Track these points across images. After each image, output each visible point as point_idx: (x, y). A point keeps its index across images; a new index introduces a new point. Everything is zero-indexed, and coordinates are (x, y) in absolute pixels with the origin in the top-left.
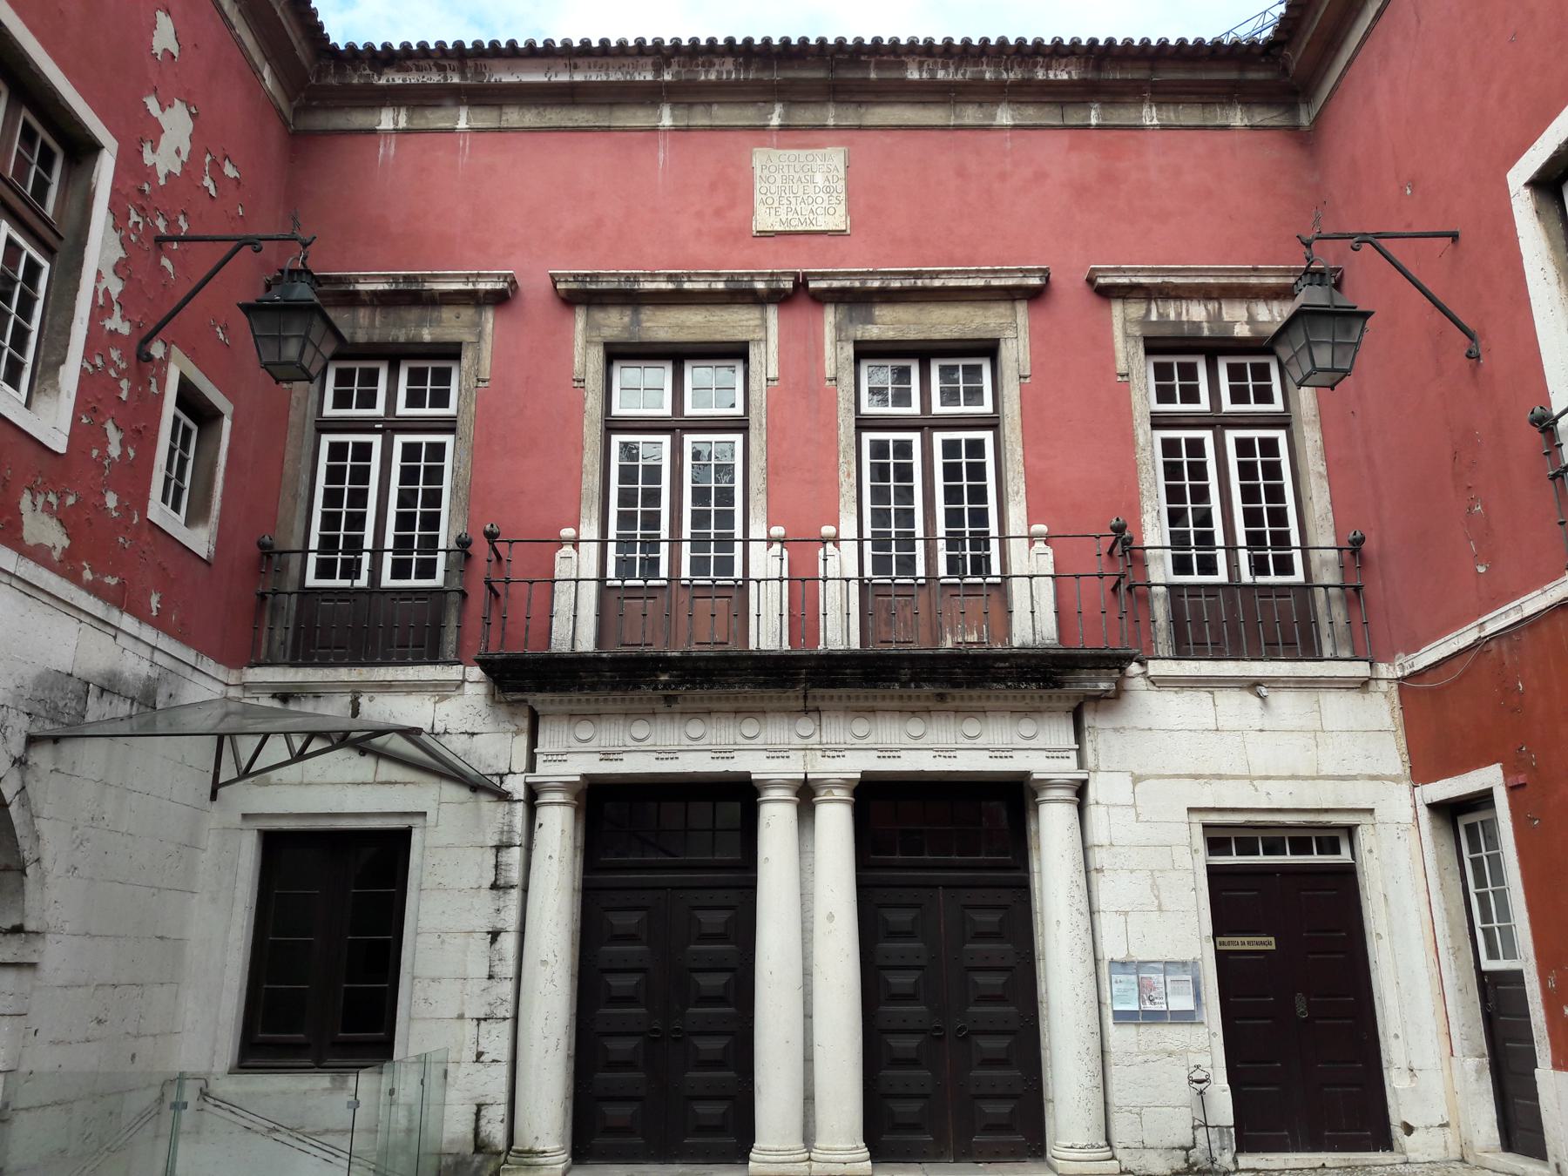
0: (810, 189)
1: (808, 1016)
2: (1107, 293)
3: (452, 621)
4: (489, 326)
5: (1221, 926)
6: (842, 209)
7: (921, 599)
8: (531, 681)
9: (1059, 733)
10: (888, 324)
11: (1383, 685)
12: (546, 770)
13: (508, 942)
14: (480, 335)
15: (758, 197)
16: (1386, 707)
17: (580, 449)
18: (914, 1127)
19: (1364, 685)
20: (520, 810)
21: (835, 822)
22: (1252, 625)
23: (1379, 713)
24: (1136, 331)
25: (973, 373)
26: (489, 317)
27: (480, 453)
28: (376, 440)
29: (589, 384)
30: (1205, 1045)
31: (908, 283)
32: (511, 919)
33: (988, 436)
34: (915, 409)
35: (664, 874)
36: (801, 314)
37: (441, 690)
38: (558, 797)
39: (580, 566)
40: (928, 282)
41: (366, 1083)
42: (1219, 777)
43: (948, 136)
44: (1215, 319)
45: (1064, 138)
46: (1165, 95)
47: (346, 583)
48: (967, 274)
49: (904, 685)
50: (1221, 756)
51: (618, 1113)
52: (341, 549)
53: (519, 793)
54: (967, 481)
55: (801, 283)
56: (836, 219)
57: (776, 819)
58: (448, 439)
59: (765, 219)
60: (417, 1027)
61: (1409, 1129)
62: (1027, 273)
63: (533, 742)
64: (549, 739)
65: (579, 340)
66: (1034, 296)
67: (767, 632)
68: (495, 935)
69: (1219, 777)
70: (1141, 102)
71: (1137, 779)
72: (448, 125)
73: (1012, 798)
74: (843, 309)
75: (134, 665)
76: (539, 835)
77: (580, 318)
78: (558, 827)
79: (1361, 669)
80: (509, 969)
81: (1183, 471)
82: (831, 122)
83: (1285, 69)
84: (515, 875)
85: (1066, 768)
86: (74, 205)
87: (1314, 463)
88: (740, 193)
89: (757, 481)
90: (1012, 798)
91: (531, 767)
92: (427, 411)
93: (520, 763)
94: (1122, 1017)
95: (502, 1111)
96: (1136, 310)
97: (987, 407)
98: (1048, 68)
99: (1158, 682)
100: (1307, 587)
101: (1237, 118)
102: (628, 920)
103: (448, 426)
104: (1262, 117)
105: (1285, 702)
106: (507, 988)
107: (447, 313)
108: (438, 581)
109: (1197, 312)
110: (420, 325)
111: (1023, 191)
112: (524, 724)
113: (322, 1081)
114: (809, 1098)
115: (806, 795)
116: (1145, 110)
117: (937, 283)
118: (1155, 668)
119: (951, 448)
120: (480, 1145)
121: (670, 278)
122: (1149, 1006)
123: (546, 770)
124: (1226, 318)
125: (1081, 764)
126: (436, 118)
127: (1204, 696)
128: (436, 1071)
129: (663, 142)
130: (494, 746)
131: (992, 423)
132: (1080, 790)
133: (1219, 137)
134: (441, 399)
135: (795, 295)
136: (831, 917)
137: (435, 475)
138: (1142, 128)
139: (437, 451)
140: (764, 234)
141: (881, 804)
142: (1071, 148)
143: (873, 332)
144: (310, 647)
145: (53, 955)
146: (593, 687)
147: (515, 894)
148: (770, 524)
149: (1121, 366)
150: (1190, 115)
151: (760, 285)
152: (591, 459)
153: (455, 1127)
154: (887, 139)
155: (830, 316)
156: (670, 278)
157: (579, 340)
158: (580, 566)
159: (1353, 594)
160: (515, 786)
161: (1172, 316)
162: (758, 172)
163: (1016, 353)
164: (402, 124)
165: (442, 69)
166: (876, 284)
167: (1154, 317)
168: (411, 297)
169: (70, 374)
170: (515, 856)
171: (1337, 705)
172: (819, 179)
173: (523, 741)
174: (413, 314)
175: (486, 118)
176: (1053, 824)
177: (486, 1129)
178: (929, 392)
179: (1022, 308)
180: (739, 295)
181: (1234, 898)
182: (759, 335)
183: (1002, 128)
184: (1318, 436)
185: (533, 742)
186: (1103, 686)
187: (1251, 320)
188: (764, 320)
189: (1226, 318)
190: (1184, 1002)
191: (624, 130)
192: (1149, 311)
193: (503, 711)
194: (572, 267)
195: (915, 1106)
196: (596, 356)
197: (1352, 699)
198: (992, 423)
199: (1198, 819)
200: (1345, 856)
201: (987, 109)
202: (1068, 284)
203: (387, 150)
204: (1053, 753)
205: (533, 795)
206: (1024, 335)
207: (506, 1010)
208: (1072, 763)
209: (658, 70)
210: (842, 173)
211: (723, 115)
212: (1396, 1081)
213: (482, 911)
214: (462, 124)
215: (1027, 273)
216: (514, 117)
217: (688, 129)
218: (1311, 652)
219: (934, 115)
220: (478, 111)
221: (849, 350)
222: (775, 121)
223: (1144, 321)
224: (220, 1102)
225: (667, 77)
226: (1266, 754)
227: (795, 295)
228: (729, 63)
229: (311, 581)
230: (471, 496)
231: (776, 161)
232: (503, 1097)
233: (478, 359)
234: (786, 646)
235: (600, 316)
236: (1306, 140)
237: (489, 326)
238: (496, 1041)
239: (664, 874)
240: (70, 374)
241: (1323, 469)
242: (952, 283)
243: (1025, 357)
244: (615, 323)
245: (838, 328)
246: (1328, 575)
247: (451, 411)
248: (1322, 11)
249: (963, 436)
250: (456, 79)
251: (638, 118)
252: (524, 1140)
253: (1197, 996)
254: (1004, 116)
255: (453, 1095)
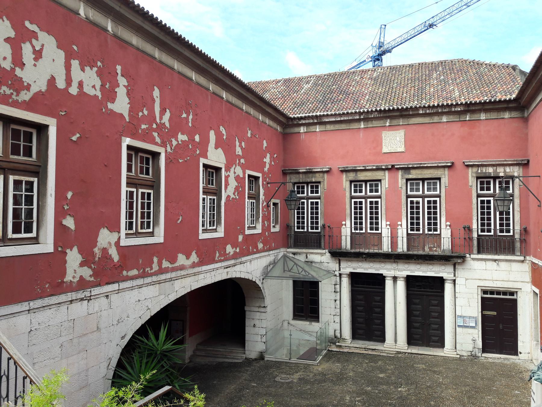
0: (396, 141)
1: (396, 319)
2: (468, 166)
3: (323, 241)
4: (326, 178)
5: (483, 308)
6: (403, 146)
7: (421, 236)
8: (338, 255)
9: (450, 269)
10: (414, 174)
11: (527, 262)
12: (342, 271)
13: (338, 302)
14: (324, 180)
15: (383, 144)
16: (528, 266)
17: (345, 204)
18: (418, 340)
19: (522, 262)
20: (338, 278)
21: (401, 285)
22: (498, 245)
23: (526, 268)
24: (475, 175)
25: (435, 184)
26: (326, 175)
27: (325, 205)
28: (305, 201)
29: (347, 190)
30: (477, 334)
31: (418, 166)
32: (338, 298)
33: (438, 199)
34: (421, 193)
35: (367, 293)
36: (393, 173)
37: (322, 254)
38: (345, 276)
39: (346, 231)
40: (423, 165)
41: (314, 324)
42: (485, 280)
43: (430, 125)
44: (495, 171)
45: (459, 124)
46: (486, 111)
47: (303, 230)
48: (433, 163)
49: (415, 260)
50: (486, 275)
51: (361, 332)
52: (301, 224)
53: (338, 275)
54: (432, 208)
55: (393, 166)
56: (402, 149)
57: (389, 284)
58: (319, 201)
59: (385, 150)
60: (323, 315)
61: (521, 353)
62: (447, 163)
63: (340, 265)
64: (343, 264)
65: (344, 180)
66: (450, 167)
67: (386, 247)
68: (335, 301)
69: (485, 280)
70: (481, 113)
71: (466, 279)
72: (313, 130)
73: (441, 281)
74: (403, 171)
75: (271, 258)
76: (342, 282)
77: (344, 176)
78: (346, 282)
79: (522, 258)
80: (339, 307)
81: (485, 207)
82: (401, 123)
83: (520, 103)
84: (338, 290)
85: (451, 276)
86: (257, 189)
87: (517, 208)
88: (379, 143)
89: (384, 212)
90: (441, 281)
91: (340, 270)
92: (315, 195)
93: (338, 269)
94: (459, 326)
95: (339, 331)
96: (475, 169)
97: (438, 192)
98: (455, 108)
99: (474, 259)
100: (513, 236)
101: (507, 115)
102: (361, 297)
103: (319, 198)
104: (514, 114)
105: (503, 265)
106: (339, 310)
107: (317, 175)
108: (319, 231)
109: (491, 170)
110: (312, 178)
111: (449, 140)
112: (338, 262)
113: (308, 323)
114: (396, 334)
115: (395, 279)
116: (482, 114)
117: (425, 165)
118: (473, 256)
119: (429, 202)
120: (336, 337)
121: (363, 167)
122: (465, 325)
123: (342, 271)
124: (498, 171)
125: (455, 276)
126: (312, 128)
127: (484, 262)
128: (328, 323)
129: (361, 134)
130: (333, 265)
131: (439, 196)
132: (454, 281)
133: (501, 121)
134: (317, 192)
135: (392, 169)
136: (400, 303)
137: (317, 208)
138: (480, 120)
139: (317, 203)
140: (385, 153)
141: (410, 280)
142: (462, 126)
143: (410, 176)
144: (297, 245)
145: (268, 309)
146: (350, 257)
147: (339, 293)
148: (386, 221)
149: (470, 184)
150: (493, 115)
151: (384, 167)
152: (348, 207)
153: (331, 333)
154: (414, 127)
155: (400, 173)
156: (363, 167)
157: (344, 180)
158: (346, 231)
159: (522, 241)
160: (337, 273)
161: (484, 171)
162: (383, 138)
163: (445, 180)
164: (305, 131)
165: (313, 119)
166: (411, 166)
167: (479, 171)
168: (310, 172)
169: (260, 219)
170: (338, 286)
171: (515, 266)
172: (398, 139)
173: (338, 265)
174: (310, 175)
175: (323, 128)
176: (448, 287)
177: (336, 334)
178: (423, 189)
179: (446, 169)
180: (379, 169)
181: (486, 304)
182: (384, 178)
183: (444, 122)
184: (519, 201)
185: (340, 265)
186: (459, 261)
187: (505, 172)
188: (385, 174)
189: (498, 171)
190: (474, 325)
191: (353, 129)
192: (478, 170)
193: (333, 258)
194: (343, 165)
195: (419, 336)
196: (348, 183)
197: (520, 264)
198: (439, 196)
199: (479, 288)
200: (515, 297)
201: (440, 117)
202: (459, 165)
203: (303, 137)
204: (449, 273)
205: (340, 275)
206: (447, 176)
207: (339, 314)
208: (453, 275)
209: (360, 116)
210: (403, 137)
211: (376, 123)
212: (520, 344)
213: (333, 296)
214: (318, 130)
215: (447, 163)
216: (329, 127)
217: (367, 128)
218: (513, 253)
219: (427, 120)
220: (321, 126)
221: (405, 181)
222: (388, 124)
223: (477, 173)
224: (291, 325)
225: (362, 117)
226: (497, 275)
227: (392, 169)
228: (376, 113)
229: (296, 230)
230: (325, 215)
231: (388, 135)
232: (339, 329)
233: (324, 185)
234: (390, 250)
235: (348, 174)
236: (526, 120)
237: (326, 178)
238: (337, 319)
239: (367, 293)
240: (260, 219)
241: (519, 210)
242: (429, 165)
243: (447, 182)
244: (352, 176)
245: (402, 176)
246: (517, 236)
247: (319, 194)
248: (539, 77)
249: (432, 199)
250: (316, 121)
251: (355, 126)
252: (343, 337)
253: (476, 324)
254: (444, 119)
255: (330, 328)
